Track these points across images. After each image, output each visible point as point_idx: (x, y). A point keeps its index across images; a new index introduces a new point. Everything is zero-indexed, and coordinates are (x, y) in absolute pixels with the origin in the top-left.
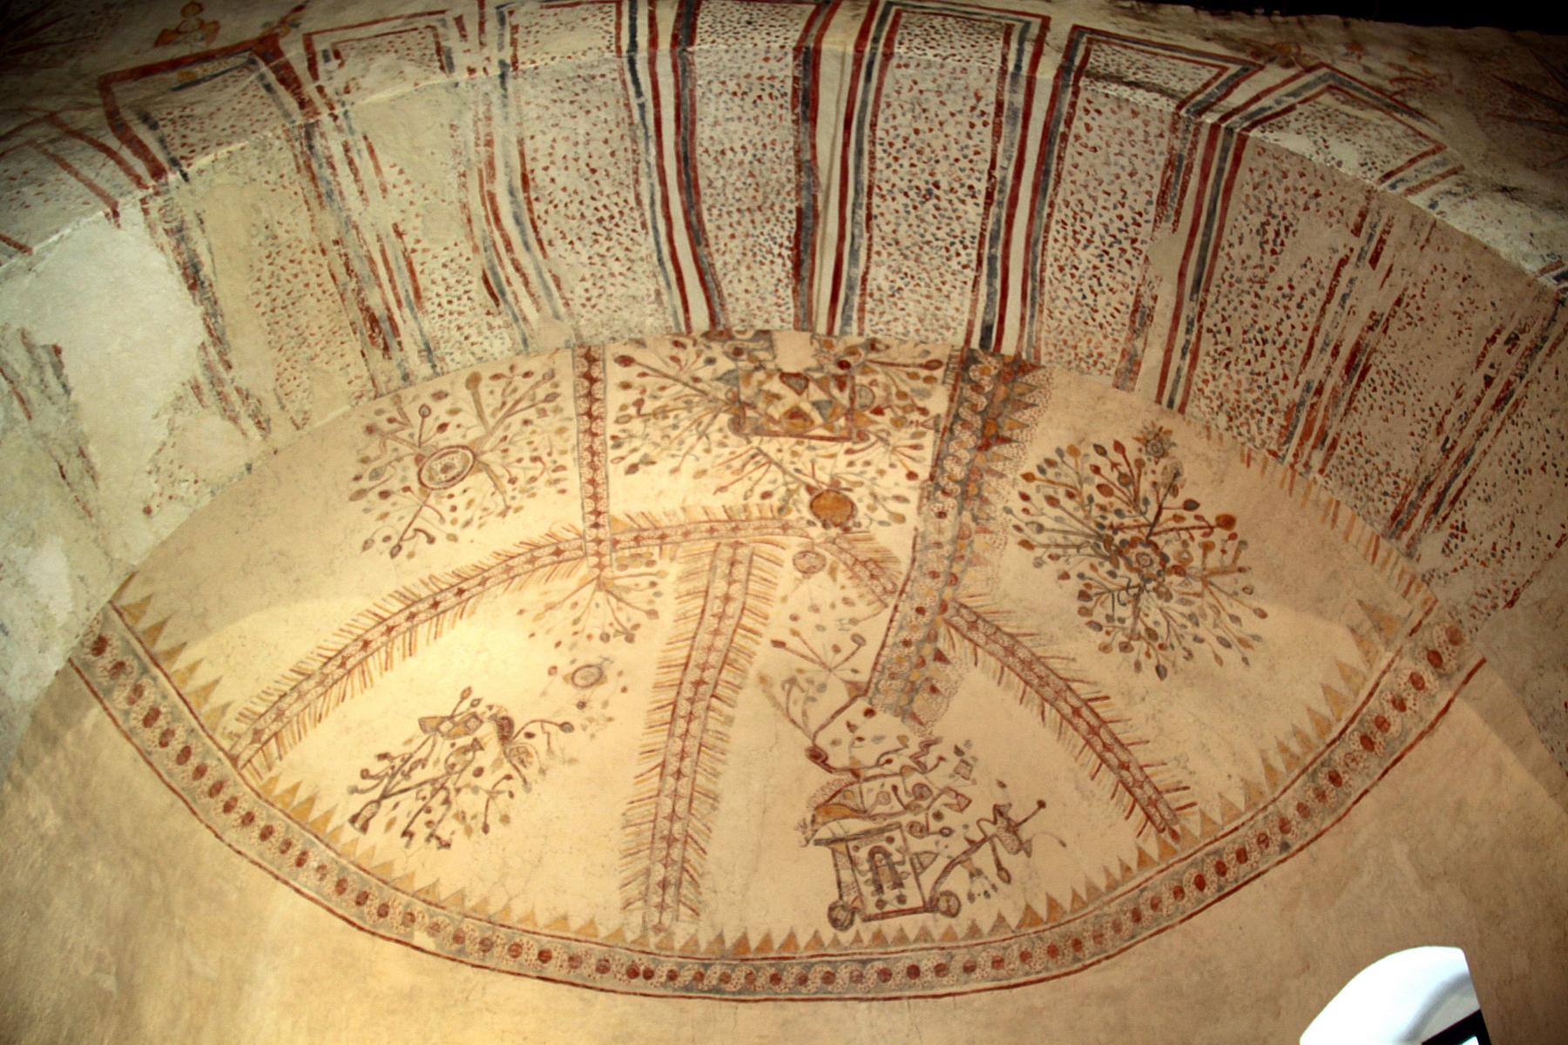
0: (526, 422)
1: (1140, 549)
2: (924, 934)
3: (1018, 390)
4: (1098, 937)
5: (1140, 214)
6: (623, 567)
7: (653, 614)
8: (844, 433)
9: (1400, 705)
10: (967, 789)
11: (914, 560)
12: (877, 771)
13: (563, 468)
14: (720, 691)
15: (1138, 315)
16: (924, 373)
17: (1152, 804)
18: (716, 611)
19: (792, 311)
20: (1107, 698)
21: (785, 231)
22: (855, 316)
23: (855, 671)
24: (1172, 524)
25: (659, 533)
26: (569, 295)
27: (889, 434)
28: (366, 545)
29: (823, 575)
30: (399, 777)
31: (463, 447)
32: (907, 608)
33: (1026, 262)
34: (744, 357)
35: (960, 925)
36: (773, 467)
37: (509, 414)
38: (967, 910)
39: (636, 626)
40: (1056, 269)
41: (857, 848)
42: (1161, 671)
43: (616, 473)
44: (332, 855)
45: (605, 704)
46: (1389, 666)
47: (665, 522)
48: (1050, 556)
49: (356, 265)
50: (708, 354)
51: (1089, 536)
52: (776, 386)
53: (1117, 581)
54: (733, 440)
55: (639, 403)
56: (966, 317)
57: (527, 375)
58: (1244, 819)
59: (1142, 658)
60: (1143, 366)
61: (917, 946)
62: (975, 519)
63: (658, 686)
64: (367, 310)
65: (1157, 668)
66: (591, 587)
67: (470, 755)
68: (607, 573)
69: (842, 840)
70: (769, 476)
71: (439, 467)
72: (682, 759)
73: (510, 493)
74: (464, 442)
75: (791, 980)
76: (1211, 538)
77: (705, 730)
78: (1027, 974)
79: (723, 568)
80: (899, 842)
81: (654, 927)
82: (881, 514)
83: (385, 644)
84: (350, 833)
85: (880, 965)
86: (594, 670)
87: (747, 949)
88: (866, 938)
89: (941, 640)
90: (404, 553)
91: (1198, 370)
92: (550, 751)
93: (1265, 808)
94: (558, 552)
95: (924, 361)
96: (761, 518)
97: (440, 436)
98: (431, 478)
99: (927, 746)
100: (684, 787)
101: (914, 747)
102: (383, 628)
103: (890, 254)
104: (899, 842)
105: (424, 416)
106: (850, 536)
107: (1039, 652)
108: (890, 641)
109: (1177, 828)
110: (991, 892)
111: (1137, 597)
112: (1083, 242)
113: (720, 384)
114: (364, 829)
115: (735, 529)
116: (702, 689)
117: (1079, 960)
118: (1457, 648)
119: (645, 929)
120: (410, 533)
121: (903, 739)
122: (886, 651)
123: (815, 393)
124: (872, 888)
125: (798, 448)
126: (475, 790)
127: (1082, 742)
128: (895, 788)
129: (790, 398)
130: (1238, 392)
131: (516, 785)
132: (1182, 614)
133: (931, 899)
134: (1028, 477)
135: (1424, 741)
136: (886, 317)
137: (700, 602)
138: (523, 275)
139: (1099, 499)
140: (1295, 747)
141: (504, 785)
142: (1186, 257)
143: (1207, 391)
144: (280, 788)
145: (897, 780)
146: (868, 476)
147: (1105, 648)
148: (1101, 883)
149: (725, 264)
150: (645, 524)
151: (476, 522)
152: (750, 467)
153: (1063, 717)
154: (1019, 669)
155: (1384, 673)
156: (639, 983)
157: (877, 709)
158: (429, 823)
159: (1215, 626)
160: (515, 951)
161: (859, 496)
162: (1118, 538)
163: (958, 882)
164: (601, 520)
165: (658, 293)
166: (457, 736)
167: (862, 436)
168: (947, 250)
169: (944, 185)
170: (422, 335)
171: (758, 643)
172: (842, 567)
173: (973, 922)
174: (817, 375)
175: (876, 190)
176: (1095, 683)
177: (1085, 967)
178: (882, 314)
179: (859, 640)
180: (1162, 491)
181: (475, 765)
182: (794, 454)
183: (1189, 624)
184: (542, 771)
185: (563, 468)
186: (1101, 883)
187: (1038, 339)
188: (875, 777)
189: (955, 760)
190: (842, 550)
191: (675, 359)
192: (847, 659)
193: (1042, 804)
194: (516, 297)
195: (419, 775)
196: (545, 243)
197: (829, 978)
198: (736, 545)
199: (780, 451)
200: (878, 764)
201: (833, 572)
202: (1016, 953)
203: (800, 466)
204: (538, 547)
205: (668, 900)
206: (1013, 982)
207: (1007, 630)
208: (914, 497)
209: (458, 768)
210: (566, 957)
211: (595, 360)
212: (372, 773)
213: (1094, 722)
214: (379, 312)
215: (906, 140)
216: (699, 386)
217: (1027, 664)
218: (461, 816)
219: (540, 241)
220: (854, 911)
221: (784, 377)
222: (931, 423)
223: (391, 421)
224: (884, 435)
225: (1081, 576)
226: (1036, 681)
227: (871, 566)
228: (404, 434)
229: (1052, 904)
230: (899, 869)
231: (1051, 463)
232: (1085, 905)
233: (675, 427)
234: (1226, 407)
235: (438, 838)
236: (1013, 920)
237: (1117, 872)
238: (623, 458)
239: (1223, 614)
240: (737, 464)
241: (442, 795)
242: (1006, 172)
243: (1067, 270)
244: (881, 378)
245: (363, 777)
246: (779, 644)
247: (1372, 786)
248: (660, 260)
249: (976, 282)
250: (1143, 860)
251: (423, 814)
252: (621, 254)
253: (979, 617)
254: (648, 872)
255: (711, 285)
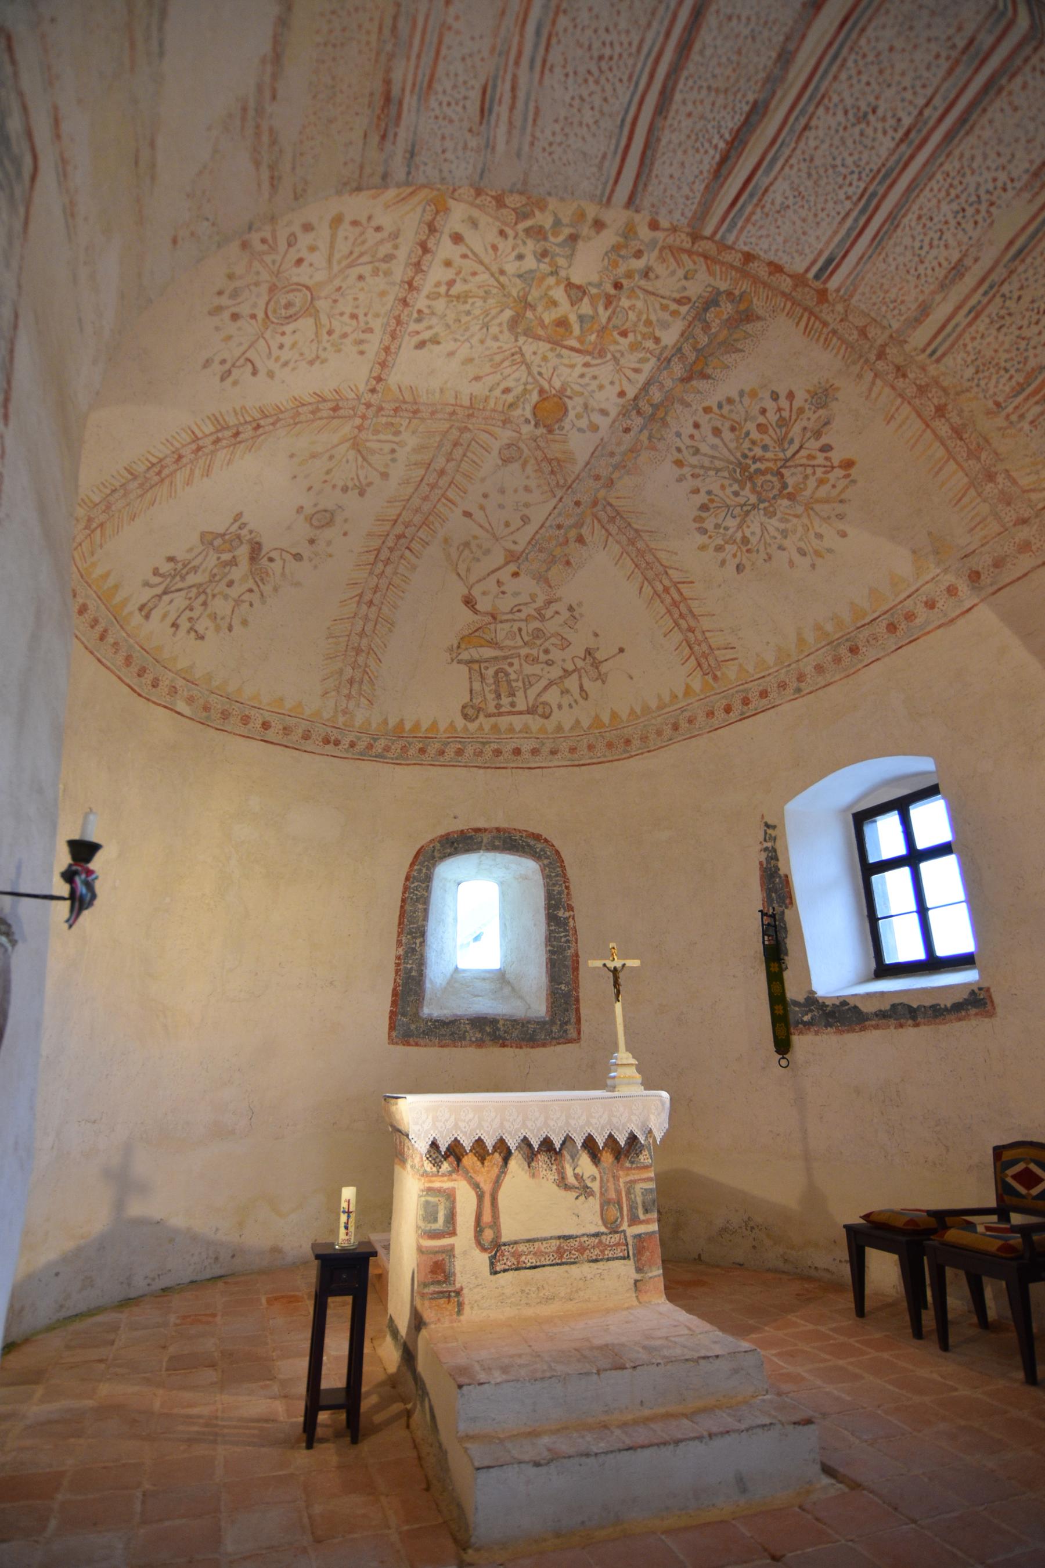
0: (361, 278)
1: (769, 477)
2: (526, 729)
3: (735, 336)
4: (644, 739)
5: (1012, 180)
6: (376, 432)
7: (385, 476)
8: (590, 348)
9: (931, 605)
10: (570, 635)
11: (588, 463)
12: (510, 617)
13: (371, 330)
14: (414, 545)
15: (953, 272)
16: (674, 306)
17: (704, 658)
18: (431, 481)
19: (694, 207)
20: (692, 582)
21: (731, 122)
22: (740, 224)
23: (515, 543)
24: (804, 461)
25: (415, 407)
26: (538, 134)
27: (622, 355)
28: (207, 363)
29: (516, 466)
30: (178, 578)
31: (308, 288)
32: (569, 501)
33: (896, 206)
34: (547, 260)
35: (550, 725)
36: (523, 367)
37: (350, 266)
38: (556, 715)
39: (370, 484)
40: (915, 216)
41: (487, 668)
42: (739, 568)
43: (408, 343)
44: (124, 634)
45: (329, 543)
46: (933, 578)
47: (424, 399)
48: (692, 475)
49: (403, 25)
50: (521, 249)
51: (731, 463)
52: (559, 294)
53: (737, 499)
54: (507, 336)
55: (451, 283)
56: (820, 246)
57: (378, 229)
58: (771, 671)
59: (729, 557)
60: (931, 317)
61: (520, 735)
62: (650, 438)
63: (370, 535)
64: (388, 82)
65: (738, 566)
66: (348, 444)
67: (228, 568)
68: (363, 435)
69: (477, 661)
70: (517, 375)
71: (283, 302)
72: (375, 592)
73: (325, 344)
74: (310, 283)
75: (433, 752)
76: (829, 476)
77: (395, 573)
78: (591, 758)
79: (447, 447)
80: (516, 666)
81: (343, 710)
82: (583, 423)
83: (191, 462)
84: (138, 618)
85: (495, 746)
86: (328, 515)
87: (403, 730)
88: (487, 728)
89: (585, 527)
90: (230, 380)
91: (974, 327)
92: (283, 574)
93: (789, 665)
94: (335, 409)
95: (677, 296)
96: (494, 410)
97: (295, 270)
98: (275, 311)
99: (549, 603)
100: (373, 612)
101: (540, 603)
102: (194, 446)
103: (799, 170)
104: (516, 666)
105: (290, 245)
106: (550, 436)
107: (653, 545)
108: (547, 524)
109: (718, 673)
110: (574, 704)
111: (747, 513)
112: (953, 196)
113: (518, 281)
114: (147, 617)
115: (470, 416)
116: (403, 540)
117: (628, 752)
118: (997, 571)
119: (336, 711)
120: (242, 360)
121: (533, 597)
122: (543, 530)
123: (585, 307)
124: (494, 696)
125: (550, 355)
126: (226, 597)
127: (663, 611)
128: (520, 630)
129: (564, 307)
130: (996, 351)
131: (255, 597)
132: (777, 529)
133: (533, 706)
134: (707, 410)
135: (942, 630)
136: (764, 232)
137: (422, 472)
138: (514, 98)
139: (755, 435)
140: (829, 627)
141: (247, 597)
142: (1024, 229)
143: (969, 348)
144: (98, 571)
145: (523, 625)
146: (590, 388)
147: (703, 548)
148: (653, 704)
149: (670, 142)
150: (408, 397)
151: (291, 365)
152: (506, 363)
153: (655, 592)
154: (633, 555)
155: (927, 583)
156: (330, 749)
157: (522, 574)
158: (190, 619)
159: (801, 539)
160: (246, 720)
161: (574, 406)
162: (753, 467)
163: (552, 696)
164: (380, 387)
165: (604, 156)
166: (223, 551)
167: (602, 354)
168: (845, 178)
169: (880, 112)
170: (415, 133)
171: (452, 511)
172: (532, 461)
173: (559, 723)
174: (594, 291)
175: (826, 101)
176: (686, 572)
177: (632, 757)
178: (761, 227)
179: (525, 520)
180: (808, 434)
181: (229, 577)
182: (545, 359)
183: (779, 537)
184: (276, 589)
185: (371, 330)
186: (653, 704)
187: (863, 279)
188: (507, 621)
189: (567, 614)
190: (538, 447)
191: (495, 248)
192: (512, 533)
193: (621, 650)
194: (497, 121)
195: (192, 579)
196: (548, 65)
197: (459, 752)
198: (464, 430)
199: (535, 353)
200: (511, 612)
201: (524, 465)
202: (585, 745)
203: (543, 371)
204: (325, 400)
205: (353, 693)
206: (581, 762)
207: (635, 526)
208: (613, 412)
209: (217, 578)
210: (281, 727)
211: (435, 231)
212: (161, 571)
213: (677, 597)
214: (396, 92)
215: (878, 54)
216: (502, 279)
217: (640, 553)
218: (214, 617)
219: (544, 62)
220: (479, 710)
221: (570, 285)
222: (657, 352)
223: (264, 241)
224: (618, 355)
225: (709, 493)
226: (644, 565)
227: (555, 463)
228: (268, 259)
229: (614, 715)
230: (514, 684)
231: (730, 401)
232: (638, 717)
233: (468, 313)
234: (979, 362)
235: (196, 632)
236: (585, 723)
237: (667, 699)
238: (418, 333)
239: (811, 532)
240: (498, 358)
241: (202, 597)
242: (932, 114)
243: (924, 220)
244: (639, 304)
245: (155, 574)
246: (467, 514)
247: (883, 657)
248: (623, 121)
249: (847, 215)
250: (688, 691)
251: (187, 611)
252: (597, 101)
253: (618, 513)
254: (341, 672)
255: (647, 162)
